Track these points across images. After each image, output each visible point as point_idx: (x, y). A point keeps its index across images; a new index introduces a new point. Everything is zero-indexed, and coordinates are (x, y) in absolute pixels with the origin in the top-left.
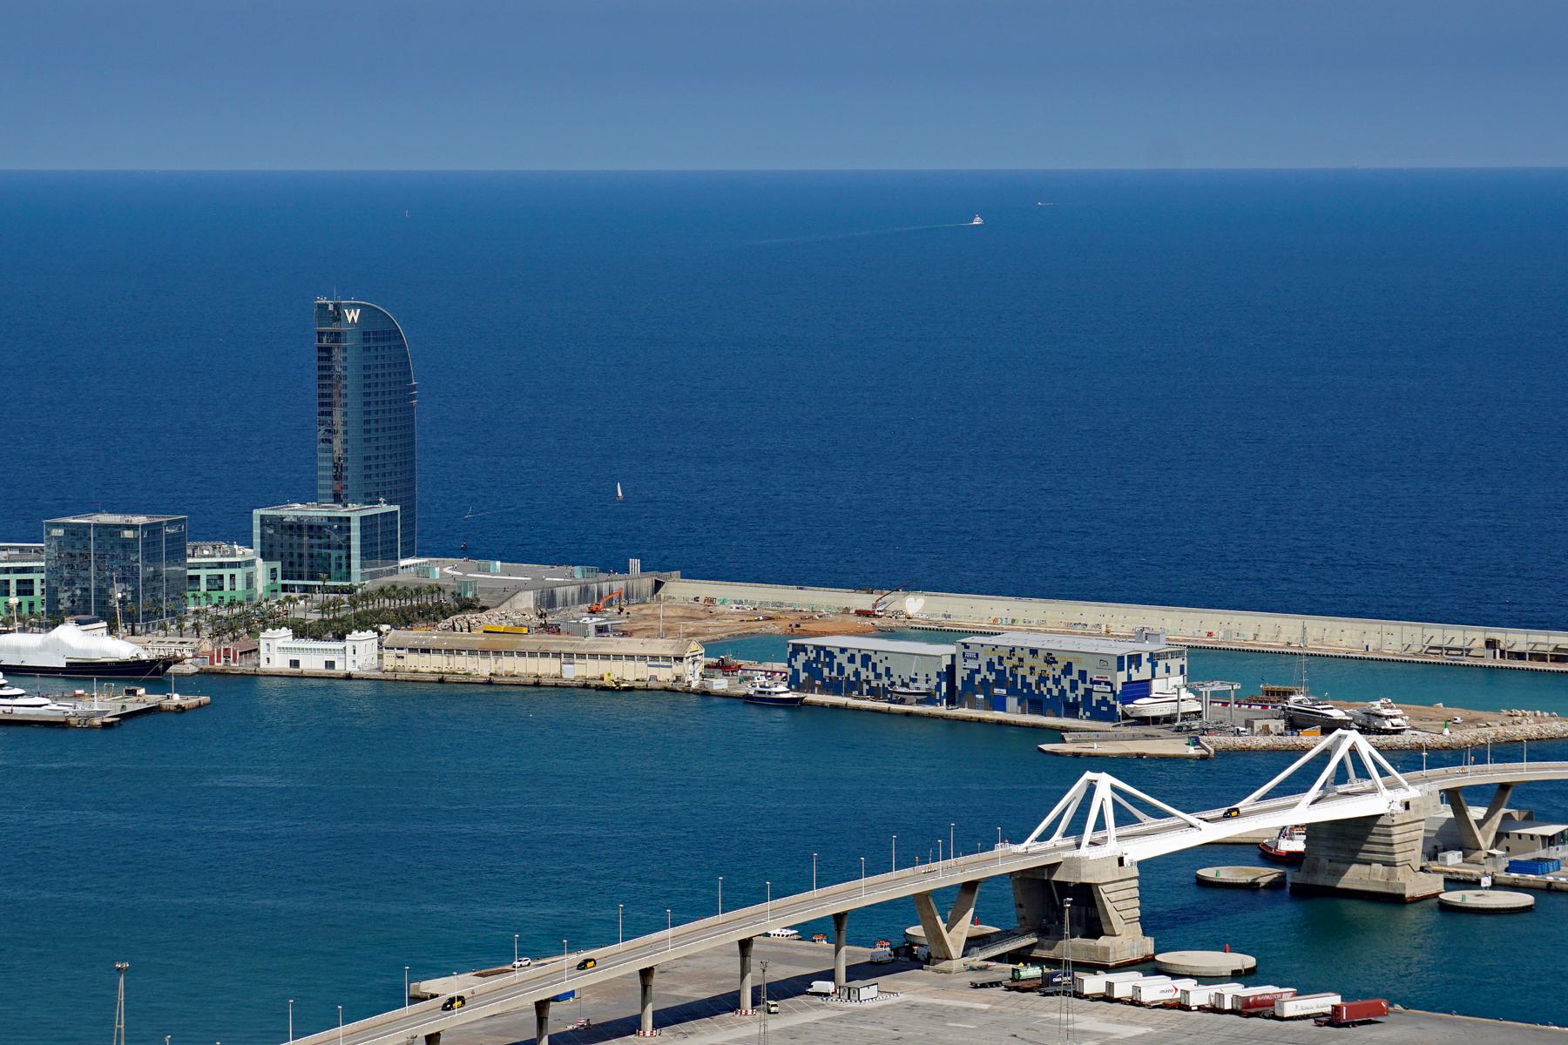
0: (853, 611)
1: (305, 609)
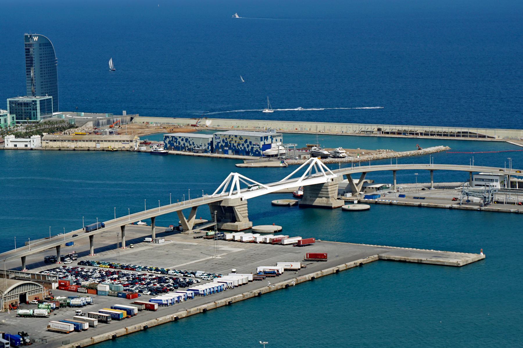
0: (190, 125)
1: (21, 129)
